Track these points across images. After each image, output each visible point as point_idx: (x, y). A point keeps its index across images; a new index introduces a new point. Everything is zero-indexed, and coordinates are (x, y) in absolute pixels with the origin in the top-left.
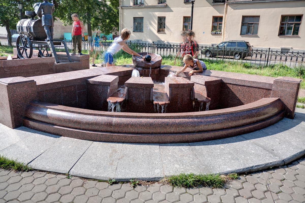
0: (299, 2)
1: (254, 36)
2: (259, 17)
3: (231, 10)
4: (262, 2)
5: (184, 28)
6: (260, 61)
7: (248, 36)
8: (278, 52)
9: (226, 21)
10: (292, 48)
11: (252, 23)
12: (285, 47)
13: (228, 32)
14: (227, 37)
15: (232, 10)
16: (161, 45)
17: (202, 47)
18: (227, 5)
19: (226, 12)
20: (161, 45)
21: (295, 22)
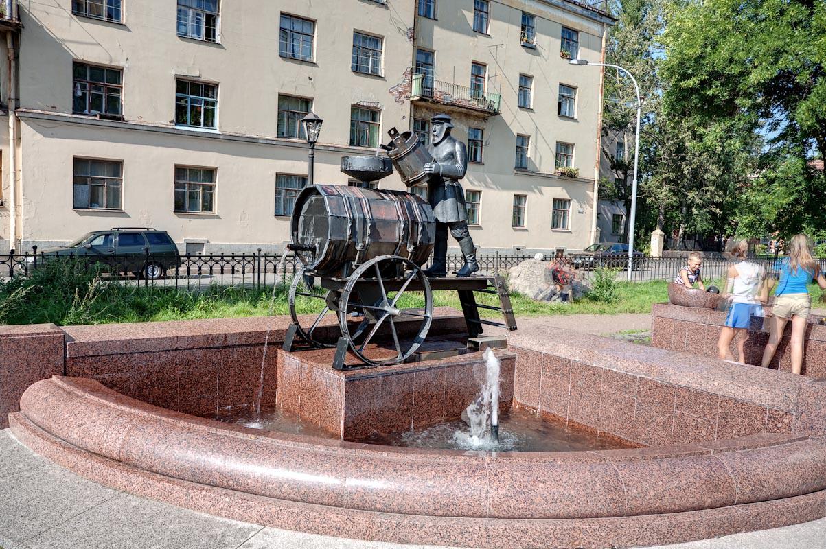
0: (168, 136)
1: (115, 214)
2: (575, 89)
3: (33, 135)
4: (112, 125)
5: (596, 20)
6: (177, 278)
7: (99, 213)
8: (235, 258)
9: (20, 166)
10: (208, 242)
11: (104, 179)
12: (193, 240)
13: (31, 202)
14: (32, 215)
15: (39, 136)
16: (481, 258)
17: (233, 257)
18: (17, 120)
19: (18, 139)
20: (481, 258)
21: (203, 181)
